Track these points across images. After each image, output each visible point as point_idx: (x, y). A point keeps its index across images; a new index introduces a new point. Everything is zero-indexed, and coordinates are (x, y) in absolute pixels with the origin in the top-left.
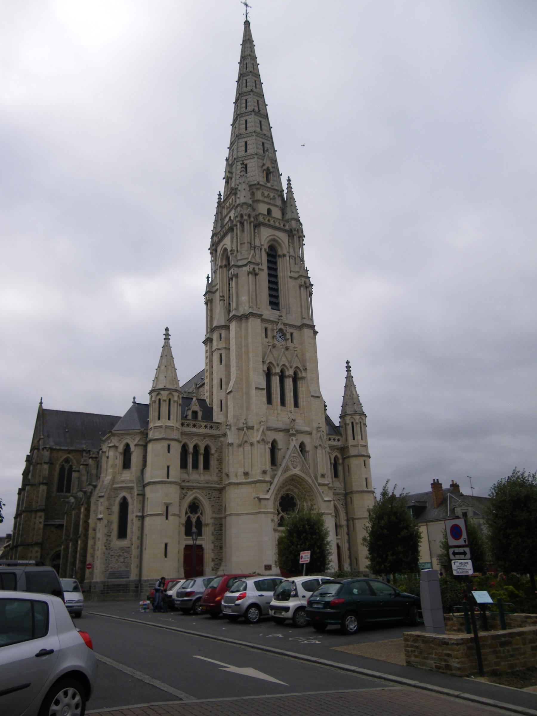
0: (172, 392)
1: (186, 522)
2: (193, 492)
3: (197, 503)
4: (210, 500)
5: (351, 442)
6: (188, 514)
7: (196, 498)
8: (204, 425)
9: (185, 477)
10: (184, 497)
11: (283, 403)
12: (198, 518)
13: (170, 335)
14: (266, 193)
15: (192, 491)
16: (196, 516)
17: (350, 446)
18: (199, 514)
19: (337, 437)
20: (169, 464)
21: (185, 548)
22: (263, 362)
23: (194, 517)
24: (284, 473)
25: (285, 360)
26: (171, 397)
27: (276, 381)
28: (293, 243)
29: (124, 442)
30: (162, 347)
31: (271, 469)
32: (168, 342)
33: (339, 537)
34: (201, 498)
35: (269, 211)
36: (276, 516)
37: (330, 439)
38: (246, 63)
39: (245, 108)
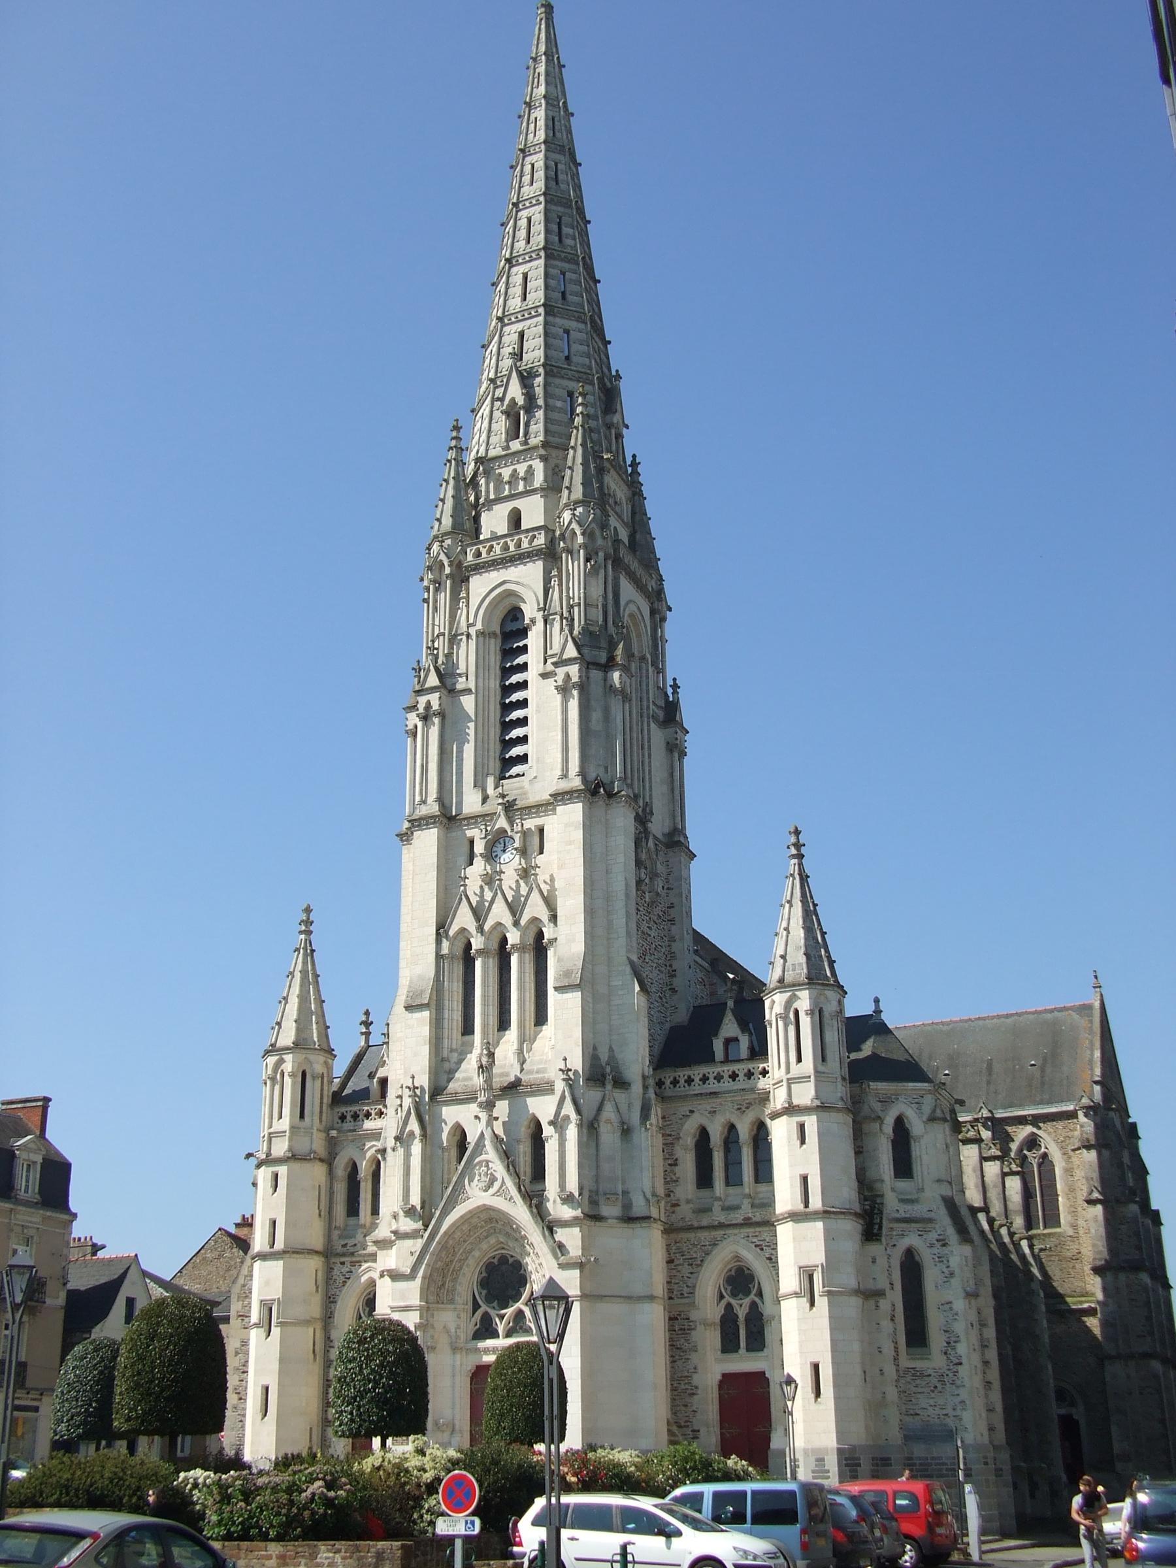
0: (826, 992)
6: (480, 1307)
8: (701, 1076)
10: (346, 1282)
12: (754, 1305)
16: (746, 1302)
18: (752, 1297)
23: (502, 1317)
31: (990, 1064)
35: (515, 519)
36: (852, 1283)
38: (536, 118)
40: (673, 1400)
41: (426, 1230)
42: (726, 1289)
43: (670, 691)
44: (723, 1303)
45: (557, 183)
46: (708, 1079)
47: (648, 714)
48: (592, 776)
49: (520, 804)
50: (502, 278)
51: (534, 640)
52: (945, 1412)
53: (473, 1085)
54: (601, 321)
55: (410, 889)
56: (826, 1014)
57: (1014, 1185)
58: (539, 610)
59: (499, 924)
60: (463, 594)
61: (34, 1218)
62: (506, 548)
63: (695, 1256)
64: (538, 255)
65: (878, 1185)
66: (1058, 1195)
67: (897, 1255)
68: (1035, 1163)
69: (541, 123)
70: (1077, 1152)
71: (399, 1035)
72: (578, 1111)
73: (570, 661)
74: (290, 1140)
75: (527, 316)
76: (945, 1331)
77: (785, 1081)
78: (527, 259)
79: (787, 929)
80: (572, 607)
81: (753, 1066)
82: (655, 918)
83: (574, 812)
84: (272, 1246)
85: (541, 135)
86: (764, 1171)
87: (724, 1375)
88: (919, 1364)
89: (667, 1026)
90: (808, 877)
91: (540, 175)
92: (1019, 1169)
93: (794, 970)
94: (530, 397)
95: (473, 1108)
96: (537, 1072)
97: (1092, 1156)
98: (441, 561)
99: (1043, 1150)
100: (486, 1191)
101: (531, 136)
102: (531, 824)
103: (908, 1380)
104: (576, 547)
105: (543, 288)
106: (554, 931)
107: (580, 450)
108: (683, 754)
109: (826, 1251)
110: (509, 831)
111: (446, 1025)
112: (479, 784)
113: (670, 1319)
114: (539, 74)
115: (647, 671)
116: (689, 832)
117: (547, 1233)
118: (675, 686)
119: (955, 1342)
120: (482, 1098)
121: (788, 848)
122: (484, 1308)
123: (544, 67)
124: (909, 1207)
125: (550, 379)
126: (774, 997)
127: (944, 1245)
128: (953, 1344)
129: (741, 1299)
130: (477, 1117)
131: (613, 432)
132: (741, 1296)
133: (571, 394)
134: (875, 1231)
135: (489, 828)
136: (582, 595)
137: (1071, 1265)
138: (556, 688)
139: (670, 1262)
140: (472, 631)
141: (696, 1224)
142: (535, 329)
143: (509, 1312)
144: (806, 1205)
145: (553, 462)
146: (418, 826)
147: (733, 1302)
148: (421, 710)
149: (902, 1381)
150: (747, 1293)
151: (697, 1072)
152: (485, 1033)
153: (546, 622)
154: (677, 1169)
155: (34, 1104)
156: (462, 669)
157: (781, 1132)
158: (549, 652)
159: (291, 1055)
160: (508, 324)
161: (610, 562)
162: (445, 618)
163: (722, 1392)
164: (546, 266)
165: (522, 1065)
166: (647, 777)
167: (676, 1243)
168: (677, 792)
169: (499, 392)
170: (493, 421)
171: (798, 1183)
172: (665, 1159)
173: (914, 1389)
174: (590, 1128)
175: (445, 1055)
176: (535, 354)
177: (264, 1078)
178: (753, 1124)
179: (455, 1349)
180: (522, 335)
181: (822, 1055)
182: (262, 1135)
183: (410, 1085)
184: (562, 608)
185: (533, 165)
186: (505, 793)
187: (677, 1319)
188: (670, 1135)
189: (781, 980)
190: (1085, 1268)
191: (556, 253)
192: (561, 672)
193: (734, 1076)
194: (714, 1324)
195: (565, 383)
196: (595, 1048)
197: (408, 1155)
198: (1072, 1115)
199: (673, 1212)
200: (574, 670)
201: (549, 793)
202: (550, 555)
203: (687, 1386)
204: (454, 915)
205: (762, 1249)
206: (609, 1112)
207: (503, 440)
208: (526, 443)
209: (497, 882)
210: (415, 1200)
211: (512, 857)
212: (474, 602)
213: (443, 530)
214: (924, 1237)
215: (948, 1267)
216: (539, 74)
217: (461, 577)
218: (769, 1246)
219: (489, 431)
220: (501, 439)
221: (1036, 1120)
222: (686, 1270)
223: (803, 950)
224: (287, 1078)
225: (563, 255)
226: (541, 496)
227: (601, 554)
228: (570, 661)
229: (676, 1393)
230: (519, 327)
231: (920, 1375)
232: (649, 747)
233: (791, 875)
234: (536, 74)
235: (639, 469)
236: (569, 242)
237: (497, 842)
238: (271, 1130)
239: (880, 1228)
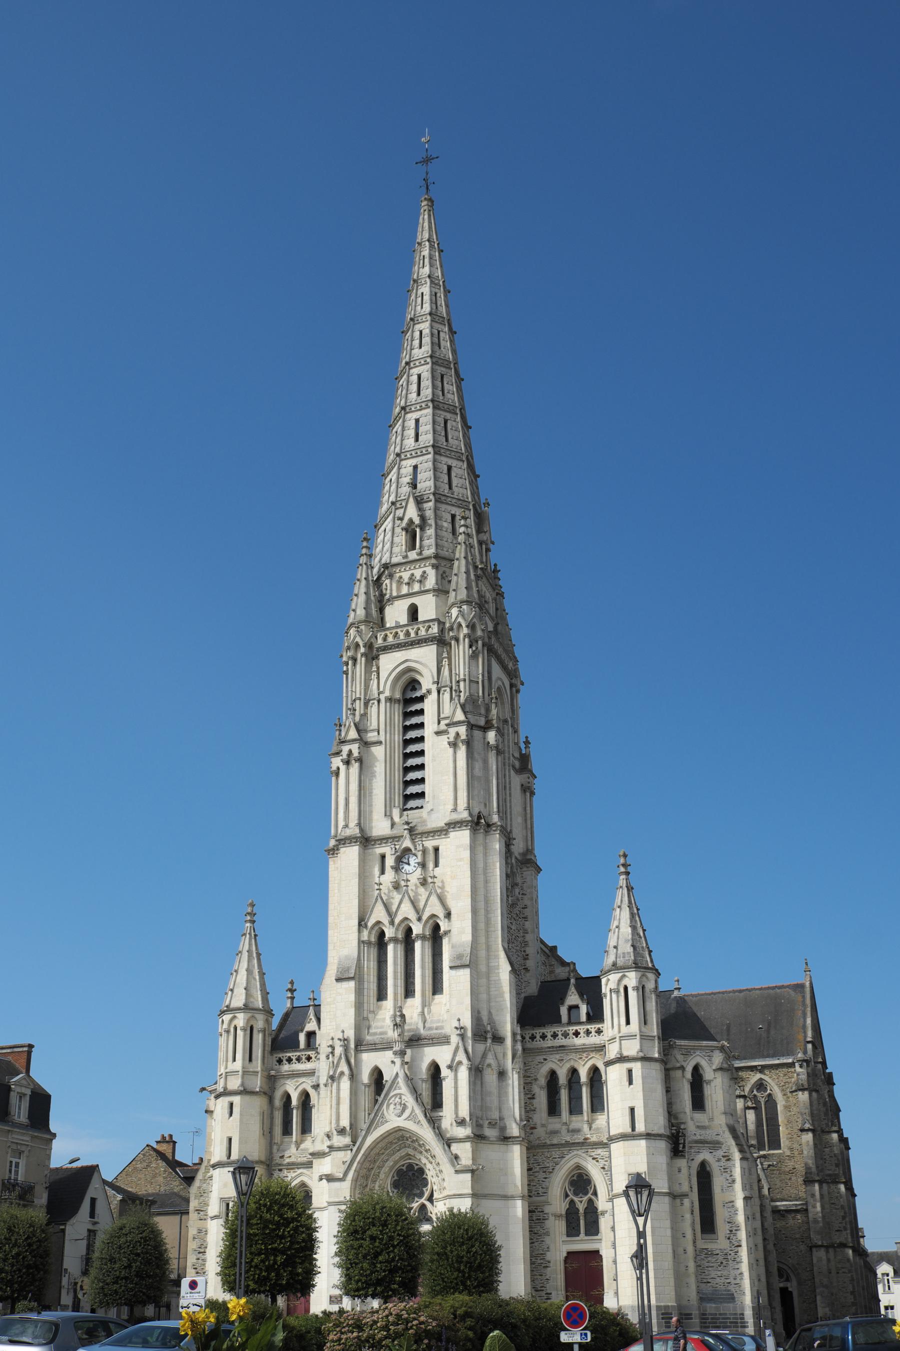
0: (647, 974)
8: (552, 1033)
12: (590, 1201)
16: (585, 1198)
18: (589, 1195)
21: (566, 1259)
27: (393, 953)
29: (567, 1066)
31: (729, 1026)
35: (413, 612)
38: (422, 293)
39: (415, 394)
40: (532, 1271)
41: (354, 1145)
42: (570, 1190)
43: (523, 746)
45: (440, 348)
46: (557, 1035)
47: (509, 763)
48: (475, 812)
49: (420, 829)
50: (398, 421)
51: (429, 705)
52: (728, 1281)
53: (388, 1038)
54: (472, 459)
55: (336, 891)
56: (647, 990)
57: (751, 1116)
58: (434, 683)
59: (406, 919)
60: (374, 669)
61: (24, 1138)
62: (408, 634)
63: (548, 1165)
64: (427, 405)
65: (681, 1116)
66: (779, 1126)
67: (695, 1165)
68: (762, 1101)
69: (427, 298)
70: (794, 1094)
71: (329, 1000)
72: (469, 1058)
73: (459, 723)
74: (243, 1078)
75: (419, 454)
76: (729, 1222)
77: (618, 1038)
78: (418, 408)
79: (618, 927)
80: (458, 682)
82: (515, 916)
83: (463, 837)
85: (427, 308)
86: (598, 1103)
88: (710, 1246)
89: (523, 996)
90: (632, 888)
91: (427, 340)
92: (754, 1105)
93: (624, 957)
94: (423, 518)
95: (389, 1054)
96: (436, 1029)
97: (804, 1097)
98: (357, 642)
99: (769, 1091)
100: (399, 1116)
101: (419, 308)
102: (430, 844)
103: (702, 1257)
104: (461, 636)
105: (431, 432)
106: (448, 926)
107: (463, 562)
108: (532, 793)
109: (648, 1163)
110: (413, 849)
111: (365, 993)
112: (388, 814)
113: (530, 1212)
114: (424, 256)
115: (508, 730)
116: (536, 852)
117: (446, 1147)
118: (527, 743)
119: (736, 1230)
120: (397, 1048)
121: (618, 867)
123: (428, 251)
124: (703, 1132)
125: (439, 505)
126: (609, 977)
127: (728, 1160)
128: (734, 1232)
130: (393, 1062)
131: (484, 546)
133: (453, 517)
134: (681, 1149)
135: (397, 847)
136: (467, 673)
137: (788, 1177)
138: (449, 743)
139: (529, 1170)
140: (382, 697)
141: (549, 1142)
142: (426, 463)
144: (633, 1128)
145: (442, 569)
146: (344, 844)
147: (576, 1199)
148: (345, 756)
149: (698, 1258)
150: (586, 1193)
151: (549, 1031)
152: (395, 999)
153: (439, 692)
154: (534, 1101)
155: (21, 1049)
156: (374, 725)
157: (614, 1076)
158: (442, 716)
159: (242, 1014)
160: (405, 459)
161: (486, 648)
162: (361, 686)
163: (567, 1265)
164: (434, 415)
165: (424, 1023)
166: (509, 811)
167: (534, 1155)
168: (529, 822)
169: (400, 513)
170: (395, 535)
171: (627, 1112)
172: (526, 1094)
173: (707, 1264)
174: (476, 1071)
175: (365, 1016)
176: (426, 484)
177: (220, 1031)
178: (569, 1071)
180: (415, 467)
181: (645, 1021)
182: (219, 1074)
183: (341, 1037)
184: (451, 682)
185: (421, 332)
186: (410, 821)
187: (534, 1212)
188: (529, 1077)
189: (614, 964)
190: (799, 1180)
191: (441, 405)
192: (453, 731)
194: (561, 1215)
195: (449, 508)
196: (479, 1012)
198: (792, 1065)
199: (532, 1133)
200: (462, 730)
201: (445, 822)
202: (442, 642)
203: (542, 1261)
204: (372, 911)
205: (597, 1161)
206: (490, 1060)
207: (404, 550)
208: (420, 554)
209: (404, 888)
210: (345, 1122)
211: (415, 869)
212: (383, 675)
213: (358, 619)
214: (714, 1154)
215: (731, 1176)
216: (424, 256)
217: (372, 655)
219: (392, 543)
220: (401, 549)
221: (762, 1069)
222: (541, 1175)
223: (630, 943)
224: (239, 1031)
225: (446, 406)
226: (433, 595)
227: (480, 643)
228: (459, 723)
229: (534, 1266)
230: (413, 462)
231: (710, 1253)
232: (510, 788)
233: (621, 887)
234: (422, 257)
235: (500, 575)
236: (449, 396)
237: (402, 857)
238: (227, 1070)
239: (684, 1147)
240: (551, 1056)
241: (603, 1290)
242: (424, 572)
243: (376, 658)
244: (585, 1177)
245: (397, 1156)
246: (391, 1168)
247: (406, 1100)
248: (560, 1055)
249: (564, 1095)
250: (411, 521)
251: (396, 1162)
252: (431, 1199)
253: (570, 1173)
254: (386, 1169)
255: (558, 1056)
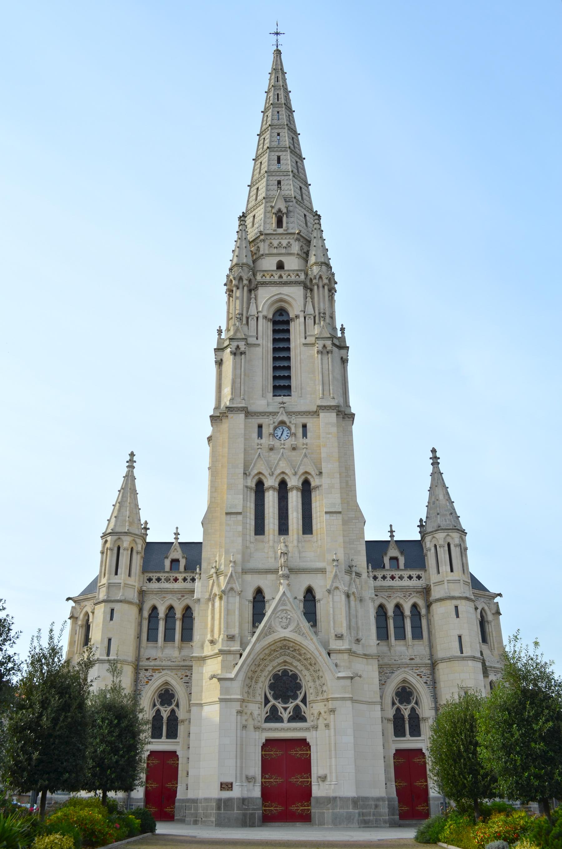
1: (394, 716)
2: (161, 674)
3: (172, 691)
4: (187, 684)
5: (434, 578)
6: (269, 702)
7: (404, 681)
9: (385, 649)
10: (148, 682)
11: (283, 529)
12: (173, 711)
13: (439, 458)
14: (275, 243)
15: (161, 672)
16: (409, 707)
17: (432, 585)
19: (414, 573)
20: (110, 636)
22: (245, 474)
23: (285, 709)
24: (264, 637)
25: (284, 465)
26: (133, 545)
28: (312, 298)
30: (431, 475)
32: (132, 472)
33: (423, 739)
34: (173, 682)
35: (280, 266)
37: (150, 580)
44: (395, 707)
81: (153, 575)
84: (108, 655)
87: (396, 750)
122: (273, 702)
129: (166, 707)
132: (166, 706)
143: (291, 706)
147: (402, 707)
150: (170, 704)
179: (256, 728)
193: (410, 578)
197: (213, 605)
205: (421, 677)
218: (425, 675)
240: (381, 593)
241: (177, 784)
242: (289, 243)
243: (256, 288)
244: (171, 692)
245: (275, 663)
246: (270, 672)
247: (291, 615)
248: (388, 593)
249: (178, 625)
250: (280, 210)
251: (274, 668)
252: (304, 701)
253: (159, 688)
254: (266, 673)
255: (386, 594)
